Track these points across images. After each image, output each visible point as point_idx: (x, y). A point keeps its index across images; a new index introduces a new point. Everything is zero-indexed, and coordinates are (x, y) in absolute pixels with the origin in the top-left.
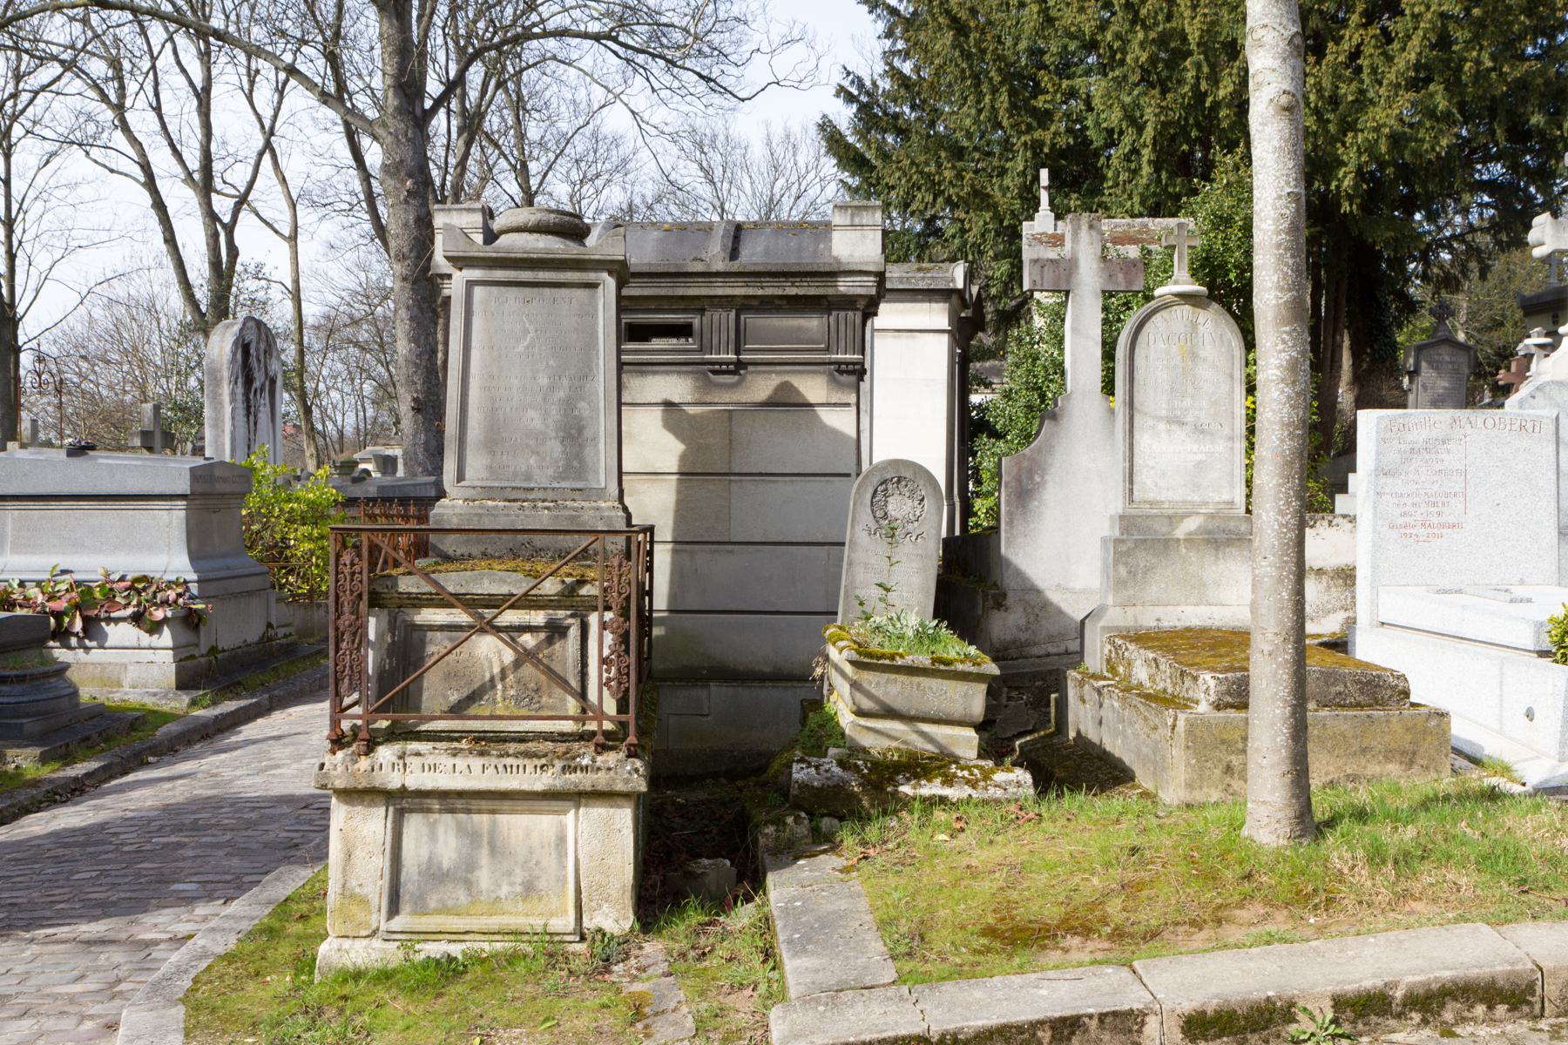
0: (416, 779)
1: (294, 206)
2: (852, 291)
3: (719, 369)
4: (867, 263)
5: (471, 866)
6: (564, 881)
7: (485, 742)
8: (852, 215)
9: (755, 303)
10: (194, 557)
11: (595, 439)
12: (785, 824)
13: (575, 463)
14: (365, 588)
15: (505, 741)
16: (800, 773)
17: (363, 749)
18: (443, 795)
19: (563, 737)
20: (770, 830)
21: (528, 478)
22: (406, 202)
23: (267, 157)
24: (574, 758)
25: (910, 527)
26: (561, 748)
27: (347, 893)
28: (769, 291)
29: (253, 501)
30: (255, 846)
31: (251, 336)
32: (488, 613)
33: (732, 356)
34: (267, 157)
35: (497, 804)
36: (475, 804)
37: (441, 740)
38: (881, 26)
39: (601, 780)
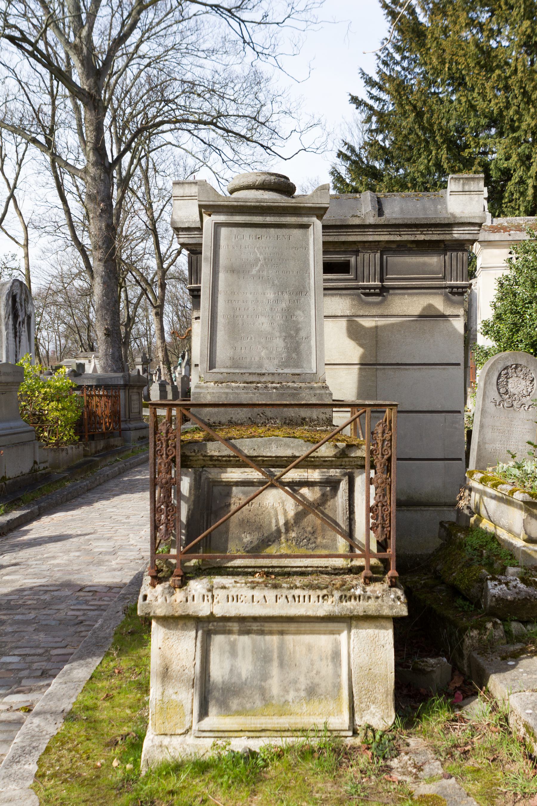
0: (220, 609)
1: (26, 228)
2: (463, 237)
3: (368, 292)
4: (474, 217)
5: (265, 676)
6: (338, 687)
7: (276, 577)
8: (463, 184)
9: (394, 246)
11: (308, 337)
12: (486, 629)
13: (294, 355)
14: (178, 453)
15: (289, 574)
16: (494, 589)
17: (178, 583)
18: (241, 619)
19: (337, 572)
20: (475, 633)
21: (260, 366)
22: (100, 215)
23: (12, 201)
24: (349, 590)
25: (524, 400)
26: (338, 580)
27: (166, 700)
28: (405, 238)
29: (23, 388)
30: (53, 623)
31: (17, 291)
32: (277, 472)
33: (378, 283)
34: (12, 201)
35: (285, 626)
36: (267, 626)
37: (238, 574)
38: (364, 116)
39: (370, 606)
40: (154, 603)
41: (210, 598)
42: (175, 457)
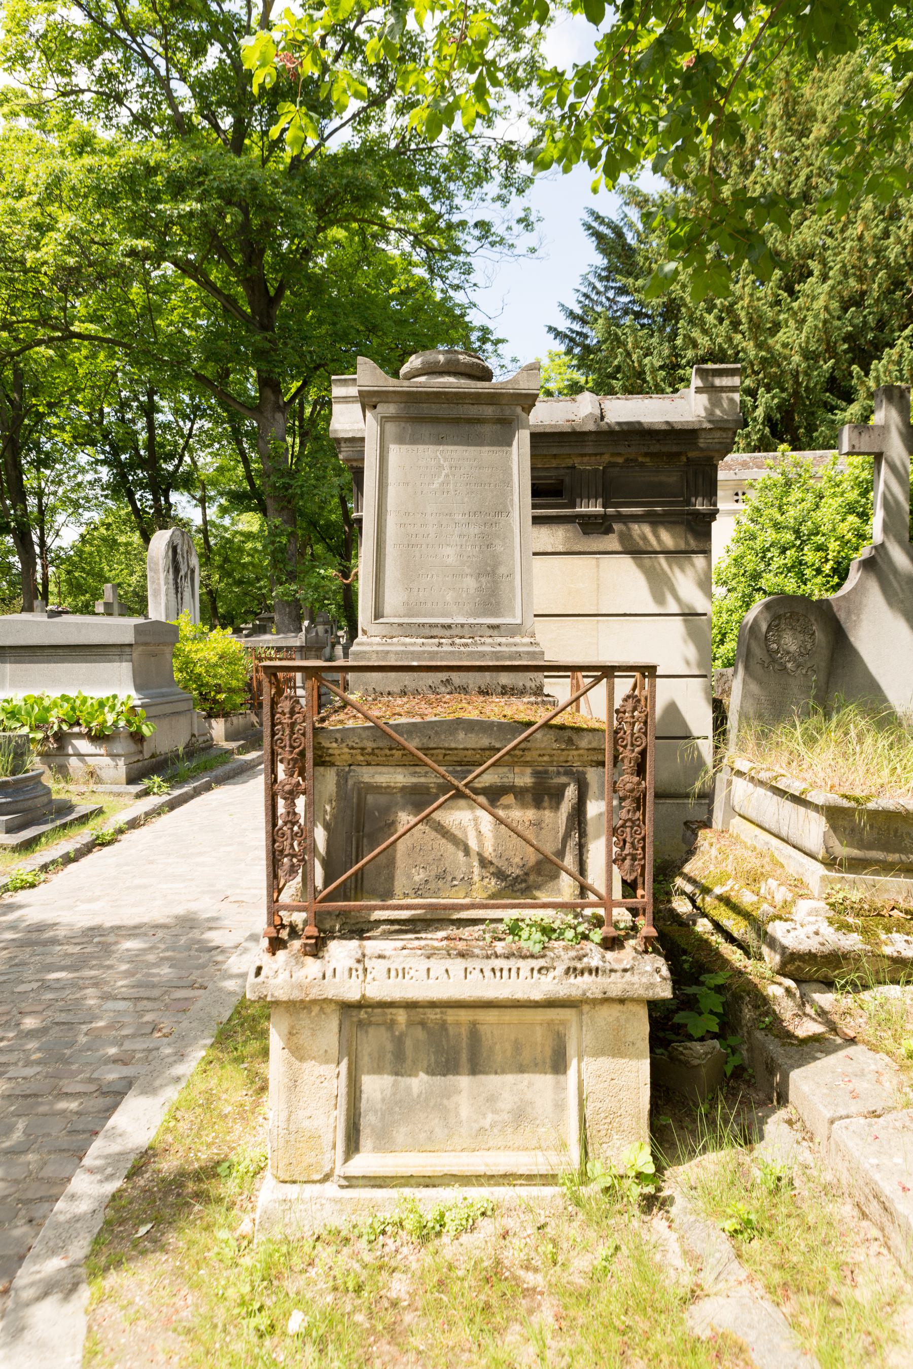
10: (138, 688)
27: (293, 1128)
39: (616, 985)
40: (272, 981)
41: (360, 972)
42: (304, 750)
